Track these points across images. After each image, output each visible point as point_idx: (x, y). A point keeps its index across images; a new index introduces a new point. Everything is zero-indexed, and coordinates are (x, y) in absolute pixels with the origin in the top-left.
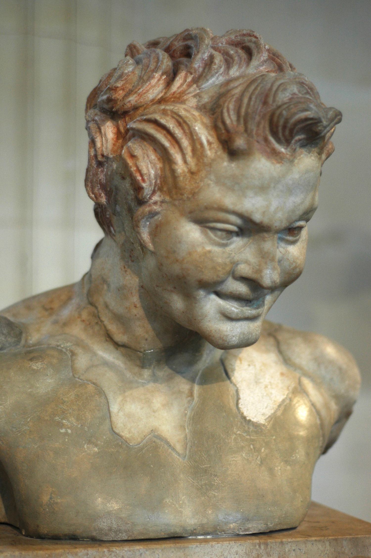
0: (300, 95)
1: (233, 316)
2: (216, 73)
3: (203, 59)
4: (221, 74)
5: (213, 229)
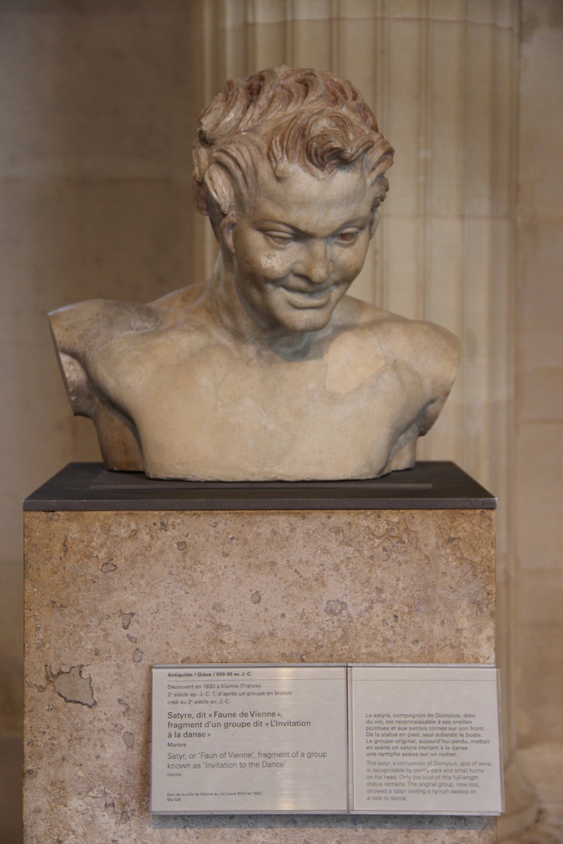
0: (330, 128)
1: (298, 305)
2: (275, 110)
3: (267, 97)
4: (280, 110)
5: (271, 236)
